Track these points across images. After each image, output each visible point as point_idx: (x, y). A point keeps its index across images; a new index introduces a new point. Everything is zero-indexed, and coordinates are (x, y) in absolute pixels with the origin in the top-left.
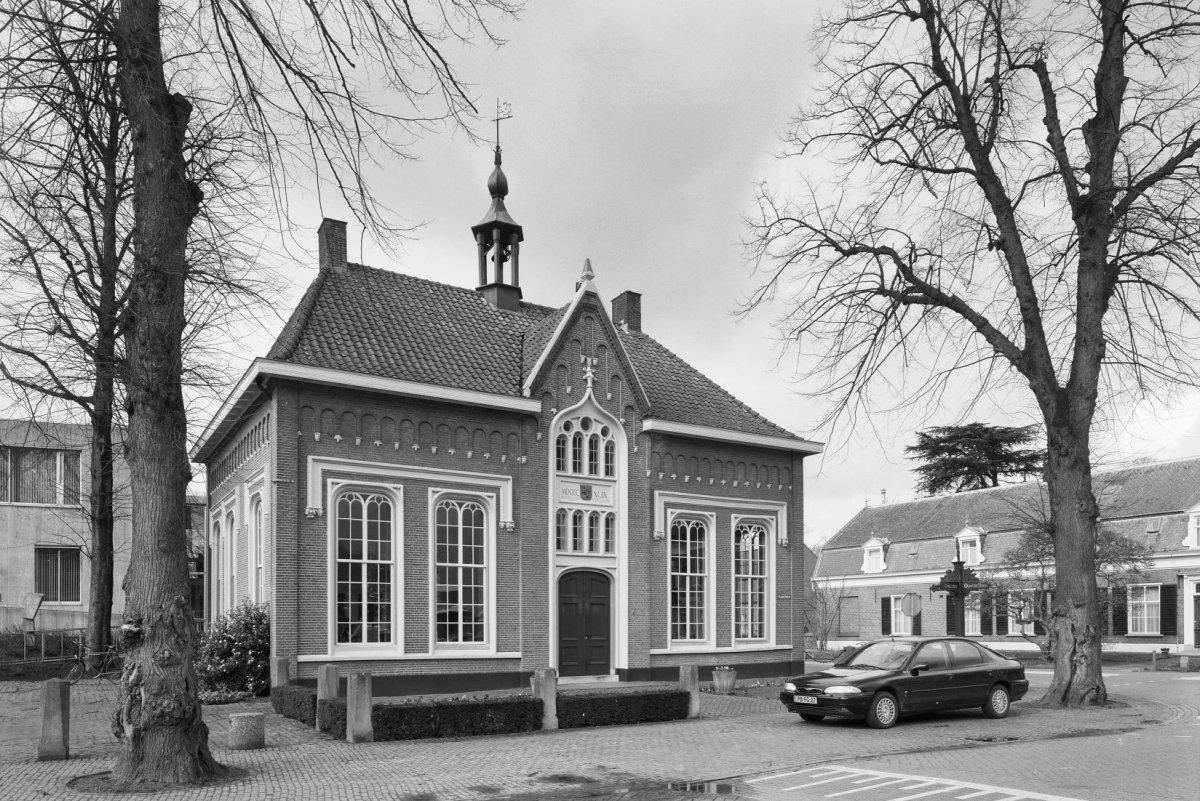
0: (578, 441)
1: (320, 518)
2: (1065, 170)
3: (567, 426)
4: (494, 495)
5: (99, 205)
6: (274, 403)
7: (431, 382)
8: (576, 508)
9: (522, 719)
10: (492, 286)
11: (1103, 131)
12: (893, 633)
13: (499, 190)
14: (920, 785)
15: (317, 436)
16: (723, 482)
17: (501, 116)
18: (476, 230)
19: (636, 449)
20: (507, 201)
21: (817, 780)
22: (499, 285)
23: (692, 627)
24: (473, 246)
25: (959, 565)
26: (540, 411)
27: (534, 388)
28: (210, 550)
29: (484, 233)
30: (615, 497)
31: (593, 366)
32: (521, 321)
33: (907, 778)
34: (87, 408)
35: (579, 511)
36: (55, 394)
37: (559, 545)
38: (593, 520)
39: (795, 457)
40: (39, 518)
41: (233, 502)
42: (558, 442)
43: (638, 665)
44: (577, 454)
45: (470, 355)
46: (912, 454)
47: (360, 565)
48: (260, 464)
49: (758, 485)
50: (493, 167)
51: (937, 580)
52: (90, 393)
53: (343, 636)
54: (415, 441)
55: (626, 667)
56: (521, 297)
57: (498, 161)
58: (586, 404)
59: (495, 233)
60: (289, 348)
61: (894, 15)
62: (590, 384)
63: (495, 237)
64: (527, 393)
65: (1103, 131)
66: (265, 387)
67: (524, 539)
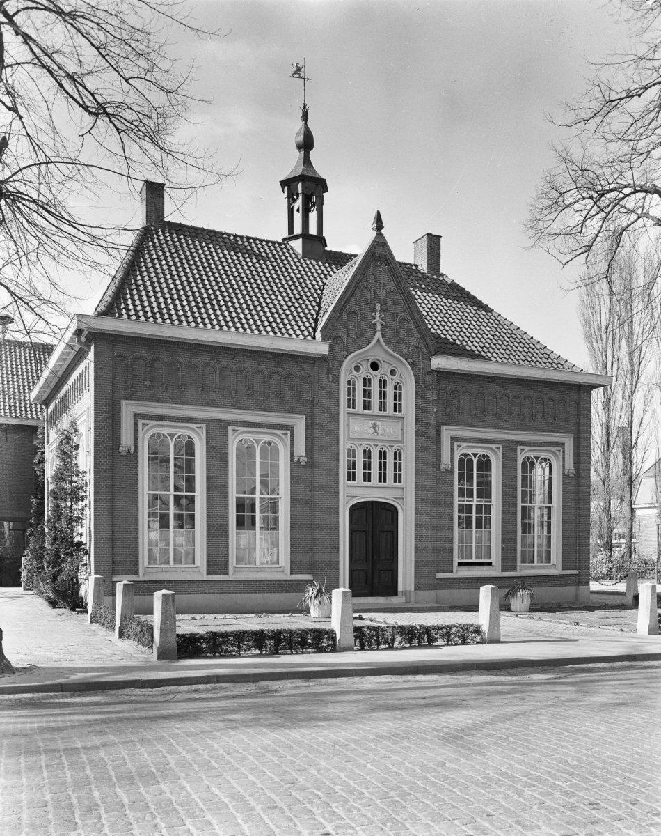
1: (133, 456)
13: (307, 144)
18: (284, 183)
20: (312, 154)
22: (305, 236)
39: (582, 390)
50: (299, 124)
56: (326, 246)
57: (305, 117)
62: (379, 328)
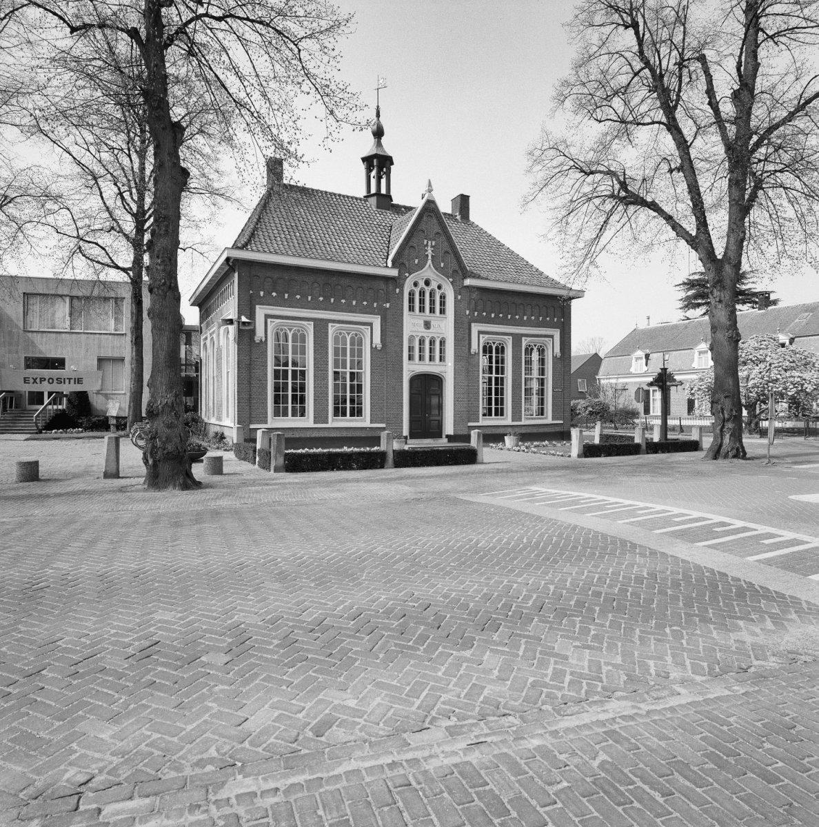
0: (422, 293)
2: (719, 121)
3: (416, 284)
4: (369, 327)
5: (136, 151)
6: (236, 275)
7: (331, 260)
8: (420, 335)
9: (374, 461)
10: (373, 195)
11: (745, 92)
12: (651, 413)
13: (379, 133)
14: (670, 514)
15: (262, 293)
16: (517, 317)
17: (380, 86)
18: (364, 160)
19: (459, 297)
20: (384, 140)
21: (582, 504)
22: (378, 194)
23: (496, 409)
24: (362, 168)
25: (664, 370)
26: (397, 275)
27: (394, 262)
28: (201, 360)
29: (368, 160)
30: (445, 327)
31: (432, 246)
32: (389, 216)
33: (642, 505)
34: (128, 274)
35: (433, 337)
36: (108, 266)
37: (411, 358)
38: (432, 342)
40: (100, 340)
41: (213, 332)
42: (410, 294)
43: (460, 433)
44: (422, 301)
45: (356, 240)
46: (678, 288)
47: (287, 371)
48: (229, 307)
49: (541, 319)
51: (650, 379)
52: (129, 265)
53: (336, 413)
54: (320, 296)
55: (452, 434)
57: (378, 115)
58: (429, 271)
59: (375, 162)
60: (249, 237)
61: (614, 26)
62: (430, 257)
63: (375, 164)
64: (390, 264)
65: (745, 92)
66: (232, 265)
67: (388, 357)
